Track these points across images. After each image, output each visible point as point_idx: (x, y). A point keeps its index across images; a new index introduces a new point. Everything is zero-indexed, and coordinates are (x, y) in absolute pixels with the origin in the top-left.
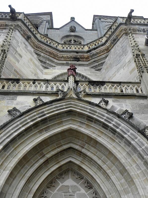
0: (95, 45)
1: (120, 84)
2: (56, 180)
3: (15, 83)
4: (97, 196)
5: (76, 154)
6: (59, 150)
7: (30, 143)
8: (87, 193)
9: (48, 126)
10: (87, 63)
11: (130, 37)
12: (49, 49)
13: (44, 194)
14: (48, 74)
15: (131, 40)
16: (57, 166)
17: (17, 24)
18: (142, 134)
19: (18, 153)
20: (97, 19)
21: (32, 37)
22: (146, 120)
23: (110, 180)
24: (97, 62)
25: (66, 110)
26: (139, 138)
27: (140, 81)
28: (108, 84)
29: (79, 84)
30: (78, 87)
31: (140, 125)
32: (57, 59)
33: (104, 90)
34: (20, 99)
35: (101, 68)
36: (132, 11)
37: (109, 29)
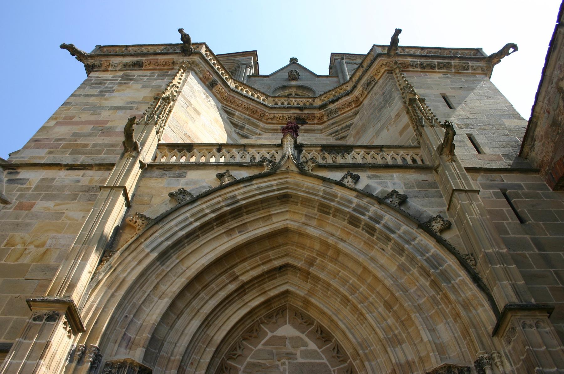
0: (334, 96)
1: (381, 149)
2: (261, 327)
3: (185, 151)
4: (338, 355)
5: (299, 278)
6: (265, 268)
7: (208, 253)
8: (321, 350)
9: (244, 222)
10: (321, 127)
11: (396, 74)
12: (250, 105)
13: (236, 351)
15: (399, 78)
18: (424, 230)
19: (187, 268)
20: (337, 59)
21: (219, 82)
22: (433, 207)
23: (366, 322)
24: (339, 124)
25: (278, 192)
27: (419, 143)
29: (304, 151)
30: (301, 156)
31: (422, 216)
32: (264, 122)
33: (349, 159)
34: (192, 175)
35: (346, 135)
36: (398, 32)
37: (359, 67)
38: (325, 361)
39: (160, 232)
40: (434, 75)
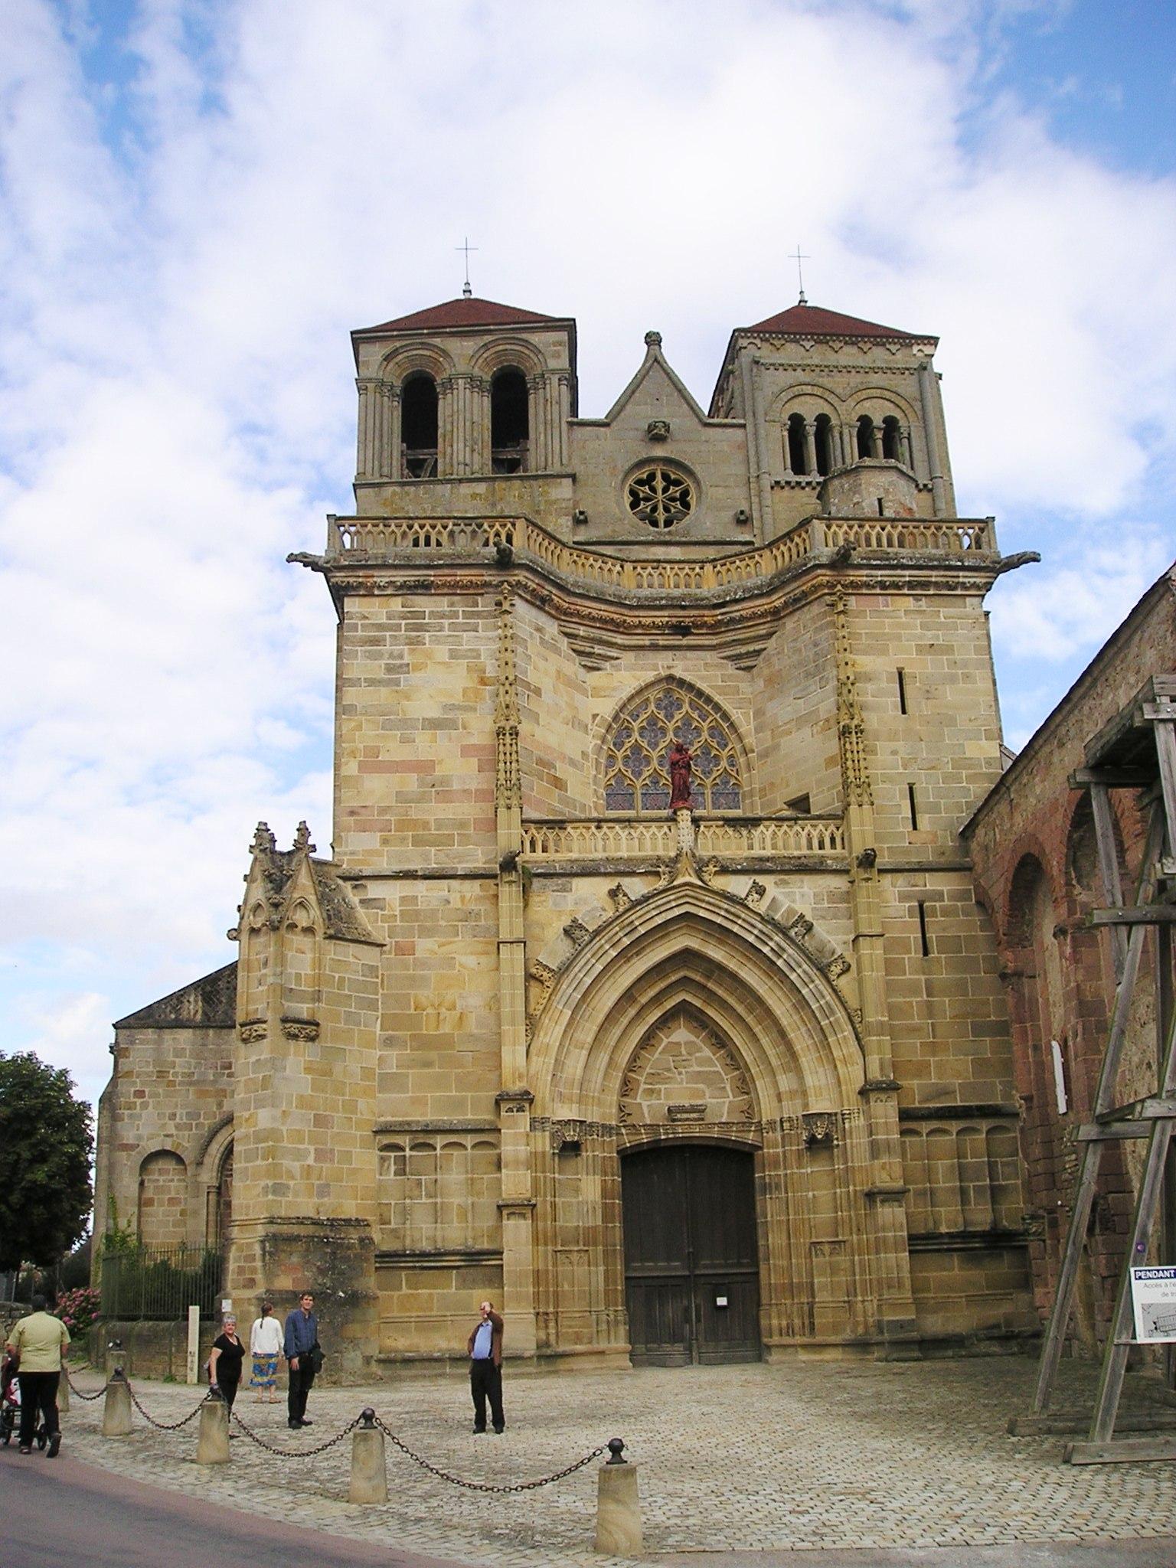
10: (714, 641)
14: (603, 693)
17: (516, 578)
26: (817, 982)
28: (767, 823)
39: (567, 982)
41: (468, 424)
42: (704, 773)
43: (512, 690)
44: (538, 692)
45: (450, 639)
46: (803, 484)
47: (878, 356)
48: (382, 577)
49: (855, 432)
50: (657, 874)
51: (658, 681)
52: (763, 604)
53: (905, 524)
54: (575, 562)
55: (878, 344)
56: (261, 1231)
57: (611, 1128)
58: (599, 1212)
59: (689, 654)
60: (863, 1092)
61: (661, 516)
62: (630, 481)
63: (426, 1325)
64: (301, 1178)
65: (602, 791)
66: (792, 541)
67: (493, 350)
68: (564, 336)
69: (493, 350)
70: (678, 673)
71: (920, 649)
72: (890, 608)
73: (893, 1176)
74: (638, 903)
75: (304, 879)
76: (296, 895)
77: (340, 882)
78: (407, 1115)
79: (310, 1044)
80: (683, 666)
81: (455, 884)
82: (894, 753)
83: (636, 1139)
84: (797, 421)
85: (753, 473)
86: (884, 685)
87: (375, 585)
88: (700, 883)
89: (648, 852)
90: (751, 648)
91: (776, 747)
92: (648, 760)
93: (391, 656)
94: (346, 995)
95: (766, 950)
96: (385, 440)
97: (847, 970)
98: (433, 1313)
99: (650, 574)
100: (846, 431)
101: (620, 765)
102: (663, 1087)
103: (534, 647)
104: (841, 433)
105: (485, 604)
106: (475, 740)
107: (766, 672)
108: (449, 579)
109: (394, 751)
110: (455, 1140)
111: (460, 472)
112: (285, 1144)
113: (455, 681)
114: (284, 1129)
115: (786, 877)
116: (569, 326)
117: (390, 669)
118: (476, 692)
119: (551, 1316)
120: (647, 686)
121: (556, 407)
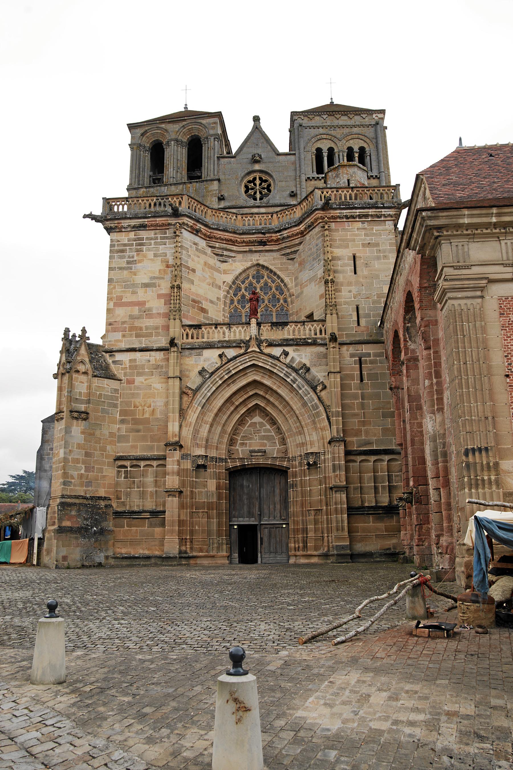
16: (245, 409)
17: (182, 221)
26: (311, 394)
28: (291, 324)
29: (262, 327)
38: (273, 434)
39: (199, 395)
40: (355, 223)
41: (175, 160)
42: (273, 306)
43: (178, 269)
44: (194, 271)
45: (154, 249)
46: (320, 178)
47: (357, 119)
48: (125, 223)
49: (345, 154)
50: (240, 347)
51: (254, 266)
52: (296, 230)
53: (357, 189)
54: (214, 215)
55: (357, 115)
56: (58, 501)
57: (223, 459)
58: (215, 496)
59: (266, 254)
60: (330, 443)
61: (258, 196)
62: (245, 181)
63: (133, 543)
64: (78, 478)
65: (227, 314)
66: (308, 200)
67: (187, 128)
68: (217, 120)
69: (187, 128)
70: (261, 262)
71: (363, 245)
72: (350, 227)
73: (341, 480)
74: (231, 360)
75: (83, 351)
76: (79, 358)
77: (104, 353)
78: (129, 452)
79: (84, 421)
80: (264, 259)
81: (153, 353)
82: (350, 291)
83: (234, 464)
84: (319, 151)
85: (298, 174)
86: (346, 261)
87: (122, 227)
88: (259, 351)
89: (238, 337)
90: (293, 250)
91: (302, 292)
92: (238, 302)
93: (129, 257)
94: (103, 401)
95: (288, 380)
96: (141, 170)
97: (325, 388)
98: (138, 538)
99: (249, 220)
100: (341, 154)
101: (236, 303)
102: (248, 442)
103: (192, 251)
104: (339, 155)
105: (169, 233)
106: (164, 291)
107: (299, 260)
108: (153, 223)
109: (128, 298)
110: (149, 463)
111: (171, 181)
112: (70, 464)
113: (157, 266)
114: (70, 458)
115: (298, 348)
116: (219, 115)
117: (128, 263)
118: (164, 271)
119: (188, 540)
120: (248, 269)
121: (212, 151)
